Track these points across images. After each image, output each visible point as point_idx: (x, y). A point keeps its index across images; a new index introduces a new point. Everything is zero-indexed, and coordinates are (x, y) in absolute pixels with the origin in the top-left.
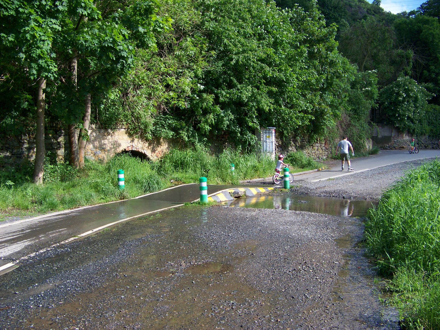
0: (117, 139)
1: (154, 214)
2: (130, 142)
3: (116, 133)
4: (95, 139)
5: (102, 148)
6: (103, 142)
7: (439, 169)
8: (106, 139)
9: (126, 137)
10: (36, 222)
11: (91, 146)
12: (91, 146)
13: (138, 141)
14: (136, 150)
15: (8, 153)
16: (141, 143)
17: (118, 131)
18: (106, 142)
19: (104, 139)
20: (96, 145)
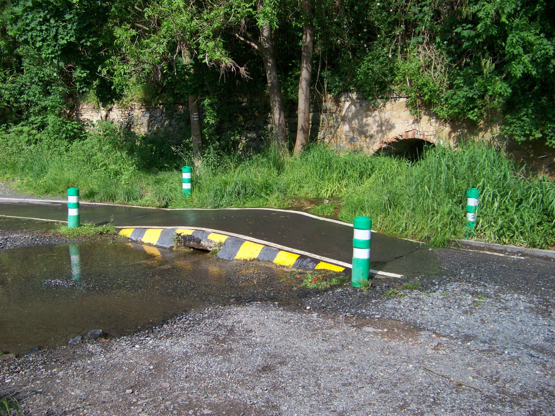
0: (389, 116)
1: (5, 218)
2: (413, 123)
3: (388, 105)
4: (355, 116)
5: (362, 131)
6: (365, 120)
7: (422, 413)
8: (370, 116)
9: (406, 114)
10: (37, 203)
11: (346, 128)
12: (346, 128)
13: (429, 120)
14: (421, 137)
15: (254, 135)
16: (434, 124)
17: (393, 102)
18: (370, 120)
19: (367, 117)
20: (354, 125)
